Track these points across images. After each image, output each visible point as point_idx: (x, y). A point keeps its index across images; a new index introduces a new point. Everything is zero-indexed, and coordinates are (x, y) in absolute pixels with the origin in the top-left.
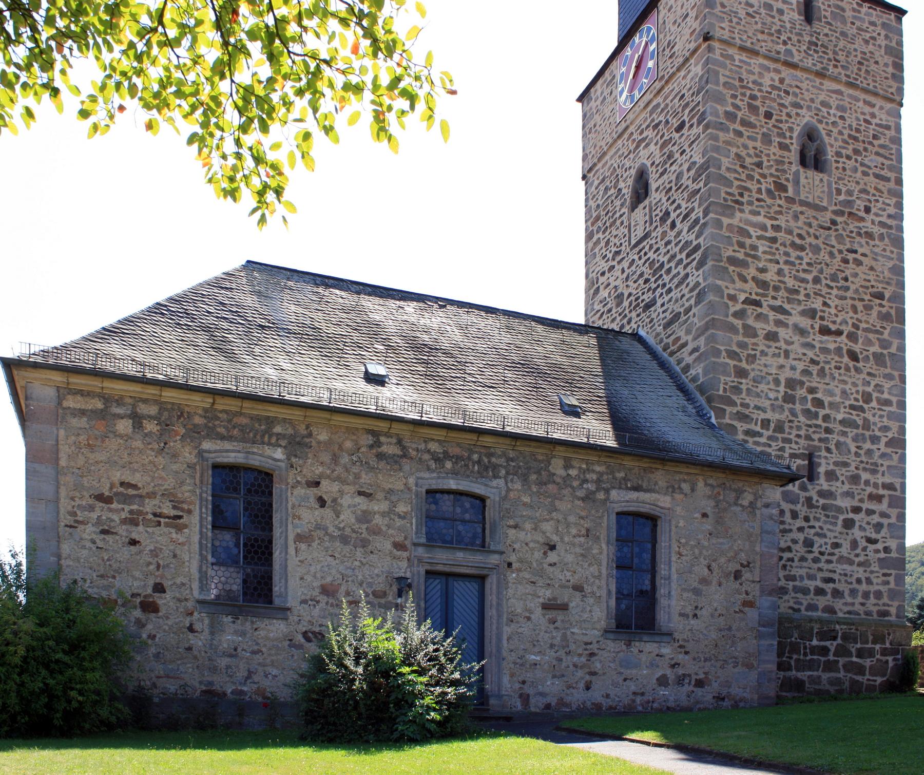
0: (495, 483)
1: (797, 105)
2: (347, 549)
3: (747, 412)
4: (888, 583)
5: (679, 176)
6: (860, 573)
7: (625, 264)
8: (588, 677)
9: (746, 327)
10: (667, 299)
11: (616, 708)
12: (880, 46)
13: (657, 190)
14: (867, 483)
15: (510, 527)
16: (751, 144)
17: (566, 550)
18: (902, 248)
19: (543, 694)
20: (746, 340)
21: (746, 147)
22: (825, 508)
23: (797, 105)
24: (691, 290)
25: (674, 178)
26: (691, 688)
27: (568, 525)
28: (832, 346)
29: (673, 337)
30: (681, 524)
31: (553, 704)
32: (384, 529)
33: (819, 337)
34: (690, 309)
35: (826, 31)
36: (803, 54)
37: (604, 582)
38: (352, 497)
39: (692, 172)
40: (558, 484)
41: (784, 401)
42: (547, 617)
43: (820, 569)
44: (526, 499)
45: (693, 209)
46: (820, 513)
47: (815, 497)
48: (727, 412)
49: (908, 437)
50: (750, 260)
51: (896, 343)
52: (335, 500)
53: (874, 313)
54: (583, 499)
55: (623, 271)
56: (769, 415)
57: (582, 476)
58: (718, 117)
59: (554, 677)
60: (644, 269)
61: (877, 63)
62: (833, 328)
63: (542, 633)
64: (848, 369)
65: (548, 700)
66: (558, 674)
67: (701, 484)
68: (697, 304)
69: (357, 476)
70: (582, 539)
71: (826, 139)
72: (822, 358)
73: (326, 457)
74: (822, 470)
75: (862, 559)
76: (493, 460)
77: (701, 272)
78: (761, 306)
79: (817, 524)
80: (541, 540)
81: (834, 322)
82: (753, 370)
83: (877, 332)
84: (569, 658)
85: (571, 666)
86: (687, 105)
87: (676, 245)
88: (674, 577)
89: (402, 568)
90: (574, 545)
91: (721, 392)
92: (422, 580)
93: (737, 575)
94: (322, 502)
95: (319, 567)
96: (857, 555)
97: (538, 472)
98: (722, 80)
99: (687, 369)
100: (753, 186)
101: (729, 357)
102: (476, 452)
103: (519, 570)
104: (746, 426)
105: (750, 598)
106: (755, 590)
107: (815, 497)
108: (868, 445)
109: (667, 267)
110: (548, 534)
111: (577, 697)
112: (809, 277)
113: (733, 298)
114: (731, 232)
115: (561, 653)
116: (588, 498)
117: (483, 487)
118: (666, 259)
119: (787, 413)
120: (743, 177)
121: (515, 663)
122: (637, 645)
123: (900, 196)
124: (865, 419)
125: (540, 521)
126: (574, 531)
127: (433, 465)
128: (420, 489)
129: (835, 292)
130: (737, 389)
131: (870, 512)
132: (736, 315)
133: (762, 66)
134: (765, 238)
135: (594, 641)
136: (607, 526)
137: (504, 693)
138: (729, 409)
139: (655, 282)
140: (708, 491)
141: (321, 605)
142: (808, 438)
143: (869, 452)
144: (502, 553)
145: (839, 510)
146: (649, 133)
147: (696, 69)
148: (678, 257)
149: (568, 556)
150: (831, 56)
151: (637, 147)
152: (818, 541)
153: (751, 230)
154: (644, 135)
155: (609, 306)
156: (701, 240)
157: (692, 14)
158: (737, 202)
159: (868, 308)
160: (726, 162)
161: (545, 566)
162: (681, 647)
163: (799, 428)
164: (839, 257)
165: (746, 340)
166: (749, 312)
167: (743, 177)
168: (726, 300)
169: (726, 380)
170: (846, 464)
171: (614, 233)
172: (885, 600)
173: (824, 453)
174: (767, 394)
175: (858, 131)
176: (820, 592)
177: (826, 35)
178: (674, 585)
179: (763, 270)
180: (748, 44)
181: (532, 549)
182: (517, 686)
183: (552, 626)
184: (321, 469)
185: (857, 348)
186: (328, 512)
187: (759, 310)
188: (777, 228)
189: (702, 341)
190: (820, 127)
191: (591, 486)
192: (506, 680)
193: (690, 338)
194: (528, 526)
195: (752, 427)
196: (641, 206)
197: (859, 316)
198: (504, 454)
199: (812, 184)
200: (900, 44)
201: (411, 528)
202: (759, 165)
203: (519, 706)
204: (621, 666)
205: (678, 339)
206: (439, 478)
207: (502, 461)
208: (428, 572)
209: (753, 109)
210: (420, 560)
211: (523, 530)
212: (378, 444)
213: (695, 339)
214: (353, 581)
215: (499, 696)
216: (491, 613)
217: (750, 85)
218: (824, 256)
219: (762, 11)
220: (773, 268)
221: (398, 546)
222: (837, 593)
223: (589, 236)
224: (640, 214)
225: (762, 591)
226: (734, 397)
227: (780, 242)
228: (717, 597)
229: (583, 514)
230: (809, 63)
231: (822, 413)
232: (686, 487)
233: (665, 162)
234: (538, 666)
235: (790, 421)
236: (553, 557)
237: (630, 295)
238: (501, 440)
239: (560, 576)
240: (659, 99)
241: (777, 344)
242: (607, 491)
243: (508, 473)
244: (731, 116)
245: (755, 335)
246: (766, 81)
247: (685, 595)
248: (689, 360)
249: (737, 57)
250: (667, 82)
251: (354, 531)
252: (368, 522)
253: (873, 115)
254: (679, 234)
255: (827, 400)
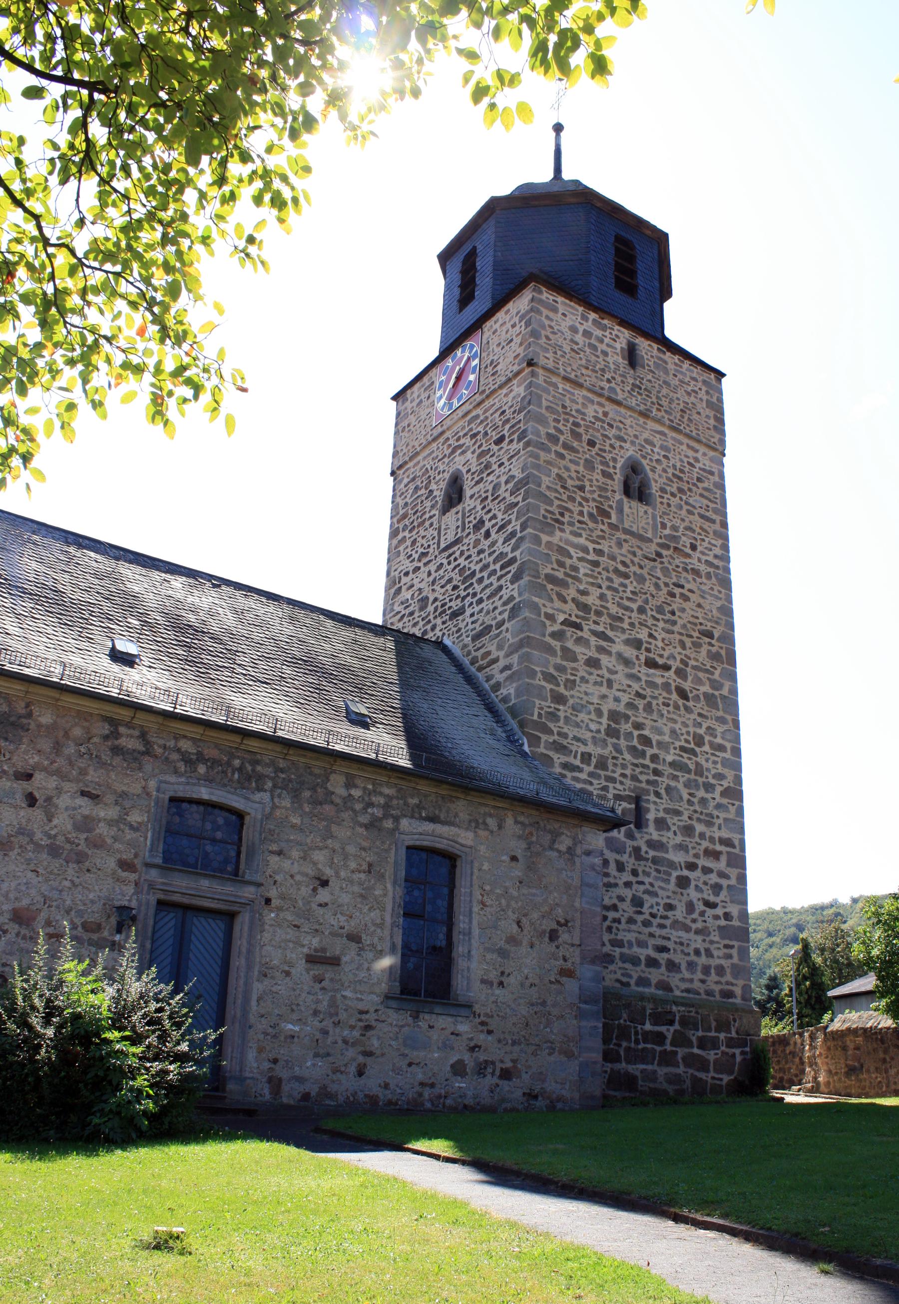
0: (258, 796)
1: (620, 439)
2: (56, 863)
3: (565, 742)
4: (730, 957)
5: (496, 487)
6: (698, 942)
7: (432, 567)
8: (361, 1059)
9: (564, 649)
10: (477, 609)
11: (396, 1104)
12: (701, 399)
13: (472, 497)
14: (702, 836)
15: (272, 852)
16: (573, 467)
17: (342, 888)
18: (730, 589)
19: (300, 1079)
20: (564, 663)
21: (568, 469)
22: (655, 861)
23: (620, 439)
24: (505, 604)
25: (490, 488)
26: (495, 1080)
27: (346, 857)
28: (659, 681)
29: (482, 651)
30: (486, 867)
31: (313, 1094)
32: (109, 841)
33: (644, 670)
34: (502, 623)
35: (649, 377)
36: (626, 394)
37: (387, 932)
38: (72, 798)
39: (510, 486)
40: (337, 805)
41: (607, 735)
42: (312, 973)
43: (651, 935)
44: (296, 820)
45: (510, 522)
46: (650, 868)
47: (644, 848)
48: (543, 741)
49: (746, 787)
50: (570, 580)
51: (727, 685)
52: (49, 799)
53: (704, 649)
54: (366, 826)
55: (429, 574)
56: (590, 748)
57: (367, 799)
58: (540, 437)
59: (316, 1055)
60: (453, 574)
61: (699, 413)
62: (660, 661)
63: (304, 995)
64: (677, 707)
65: (307, 1087)
66: (321, 1051)
67: (510, 821)
68: (511, 618)
69: (83, 772)
70: (362, 876)
71: (650, 474)
72: (648, 692)
73: (46, 745)
74: (651, 816)
75: (699, 925)
76: (259, 768)
77: (516, 586)
78: (582, 630)
79: (647, 880)
80: (311, 873)
81: (661, 656)
82: (572, 696)
83: (707, 671)
84: (338, 1030)
85: (340, 1042)
86: (508, 421)
87: (490, 555)
88: (476, 931)
89: (126, 895)
90: (352, 882)
91: (535, 717)
92: (152, 911)
93: (553, 936)
94: (31, 800)
95: (13, 885)
96: (694, 921)
97: (313, 789)
98: (545, 403)
99: (497, 687)
100: (576, 509)
101: (545, 679)
102: (238, 757)
103: (280, 909)
104: (564, 759)
105: (569, 965)
106: (575, 956)
107: (644, 848)
108: (701, 793)
109: (478, 576)
110: (320, 866)
111: (346, 1085)
112: (634, 606)
113: (551, 617)
114: (550, 549)
115: (328, 1023)
116: (373, 825)
117: (243, 801)
118: (478, 567)
119: (610, 748)
120: (565, 497)
121: (266, 1034)
122: (426, 1019)
123: (726, 538)
124: (697, 764)
125: (310, 849)
126: (353, 865)
127: (182, 766)
128: (161, 796)
129: (661, 624)
130: (553, 716)
131: (707, 871)
132: (553, 635)
133: (584, 397)
134: (588, 561)
135: (372, 1010)
136: (393, 863)
137: (247, 1075)
138: (544, 737)
139: (465, 589)
140: (518, 830)
141: (8, 936)
142: (634, 778)
143: (703, 801)
144: (259, 885)
145: (672, 865)
146: (467, 441)
147: (519, 389)
148: (492, 567)
149: (344, 895)
150: (654, 400)
151: (453, 452)
152: (649, 901)
153: (572, 551)
154: (461, 442)
155: (411, 609)
156: (517, 553)
157: (518, 340)
158: (557, 521)
159: (697, 645)
160: (546, 481)
161: (314, 906)
162: (483, 1023)
163: (624, 766)
164: (665, 590)
165: (564, 663)
166: (569, 634)
167: (565, 497)
168: (543, 618)
169: (540, 706)
170: (678, 813)
171: (422, 533)
172: (728, 977)
173: (652, 798)
174: (587, 725)
175: (682, 471)
176: (652, 963)
177: (650, 381)
178: (475, 943)
179: (584, 593)
180: (572, 376)
181: (298, 883)
182: (266, 1065)
183: (318, 986)
184: (37, 758)
185: (687, 685)
186: (37, 814)
187: (580, 633)
188: (600, 553)
189: (515, 658)
190: (644, 462)
191: (378, 812)
192: (251, 1055)
193: (501, 654)
194: (295, 854)
195: (571, 760)
196: (454, 510)
197: (688, 652)
198: (272, 763)
199: (635, 514)
200: (720, 400)
201: (144, 842)
202: (582, 488)
203: (267, 1093)
204: (405, 1045)
205: (489, 653)
206: (188, 784)
207: (269, 771)
208: (160, 903)
209: (577, 436)
210: (151, 886)
211: (289, 858)
212: (116, 735)
213: (507, 656)
214: (58, 907)
215: (241, 1080)
216: (238, 962)
217: (574, 413)
218: (649, 586)
219: (586, 349)
220: (595, 592)
221: (125, 865)
222: (672, 966)
223: (394, 533)
224: (451, 519)
225: (583, 958)
226: (551, 725)
227: (602, 566)
228: (529, 962)
229: (365, 844)
230: (633, 402)
231: (650, 752)
232: (492, 822)
233: (482, 472)
234: (296, 1039)
235: (614, 758)
236: (324, 895)
237: (436, 600)
238: (271, 746)
239: (333, 921)
240: (479, 411)
241: (600, 672)
242: (396, 819)
243: (275, 786)
244: (554, 439)
245: (575, 660)
246: (590, 411)
247: (489, 956)
248: (500, 677)
249: (560, 386)
250: (488, 397)
251: (68, 841)
252: (89, 830)
253: (697, 460)
254: (493, 544)
255: (655, 738)
